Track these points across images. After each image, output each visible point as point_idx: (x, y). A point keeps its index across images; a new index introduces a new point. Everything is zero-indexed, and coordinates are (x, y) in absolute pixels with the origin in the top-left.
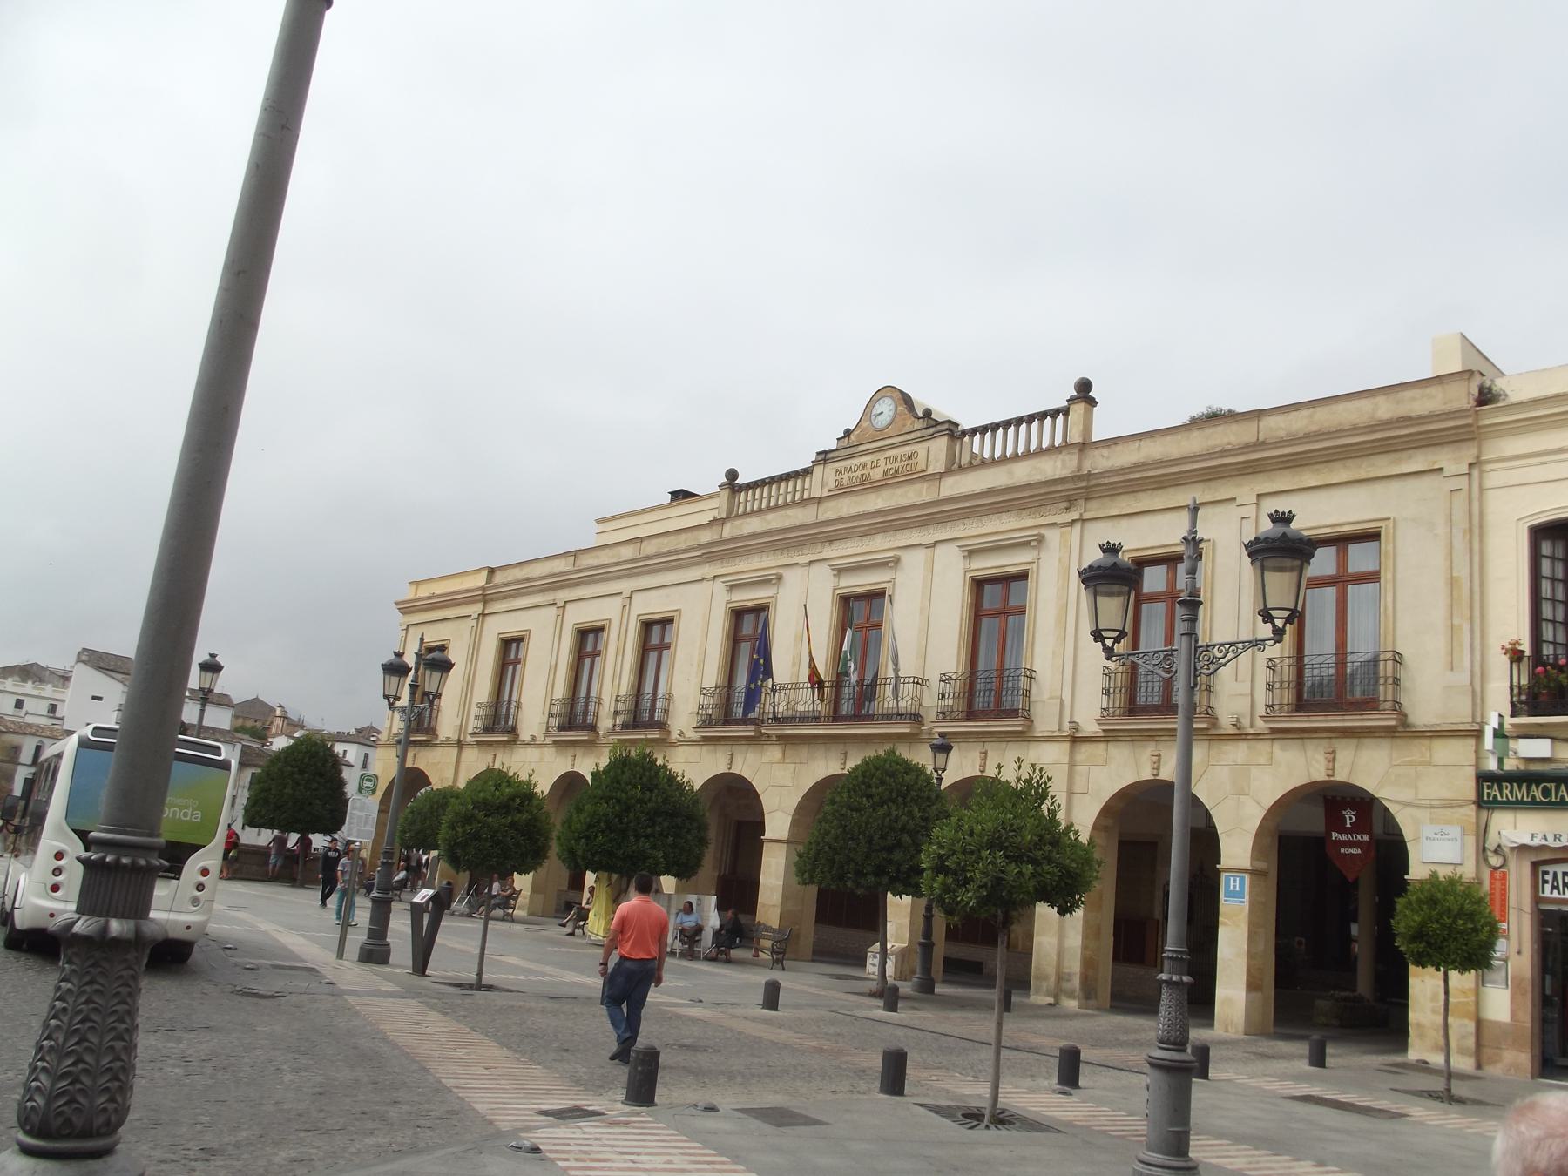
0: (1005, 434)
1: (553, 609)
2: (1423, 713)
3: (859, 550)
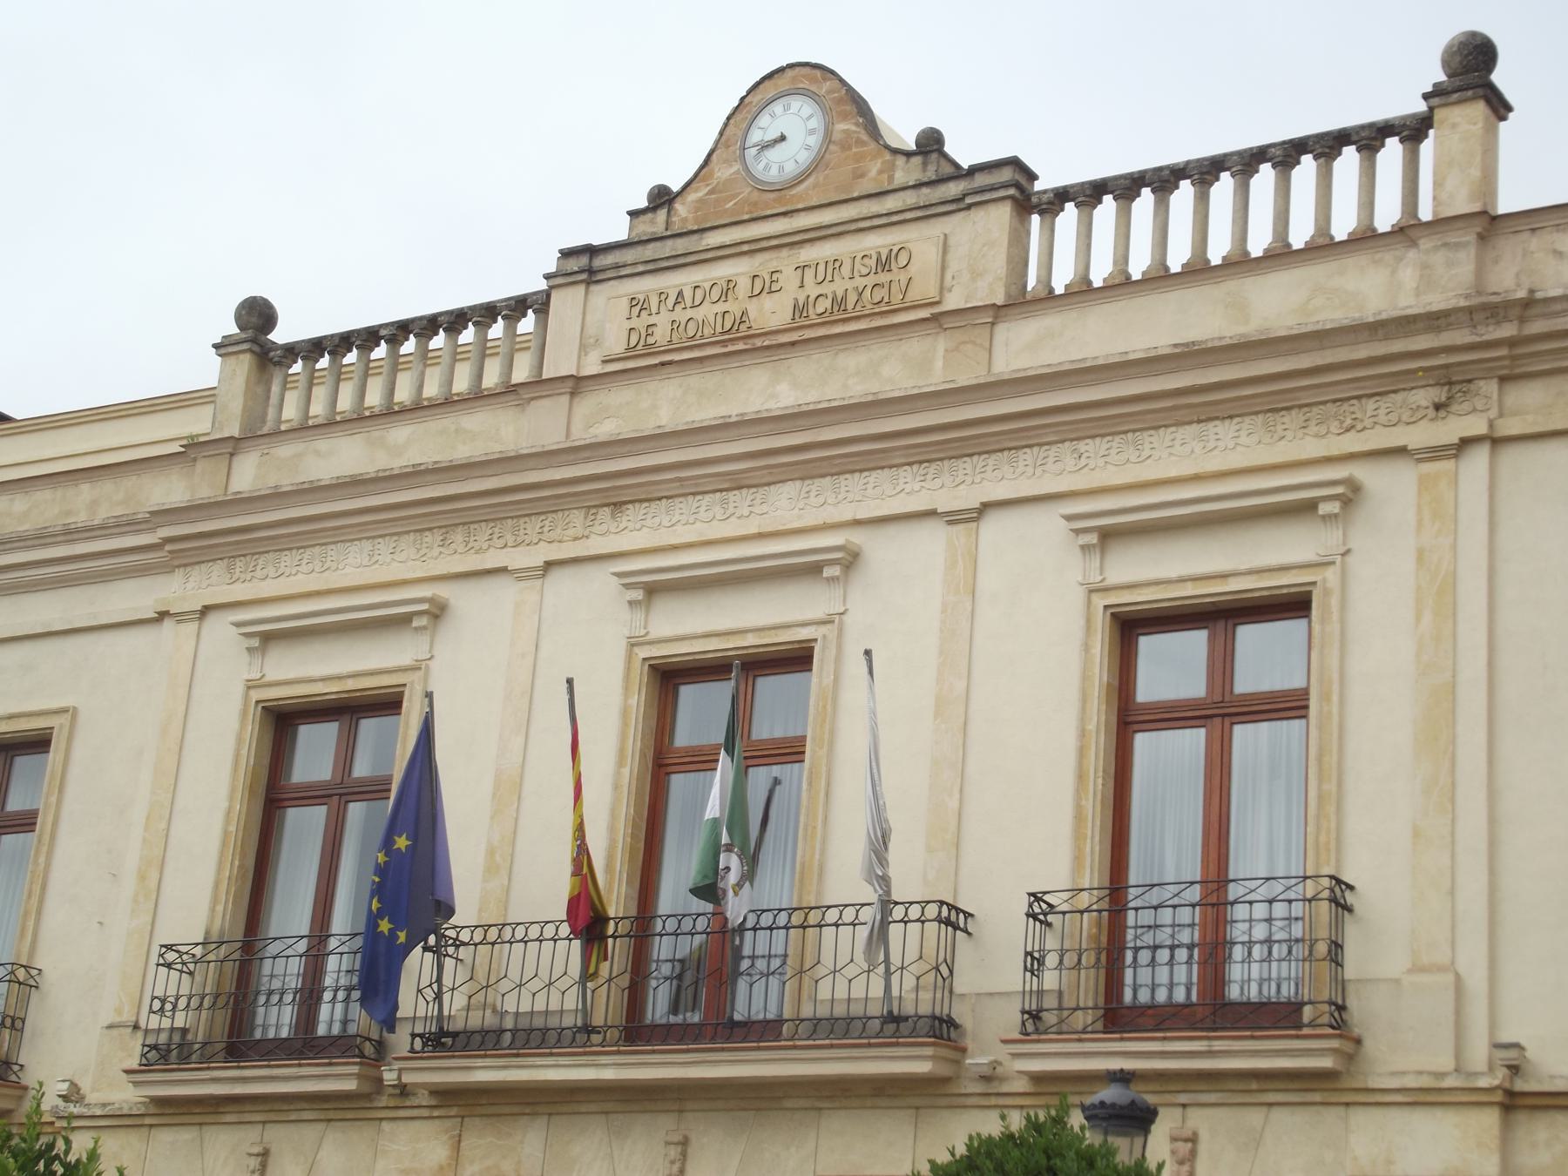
0: (1122, 257)
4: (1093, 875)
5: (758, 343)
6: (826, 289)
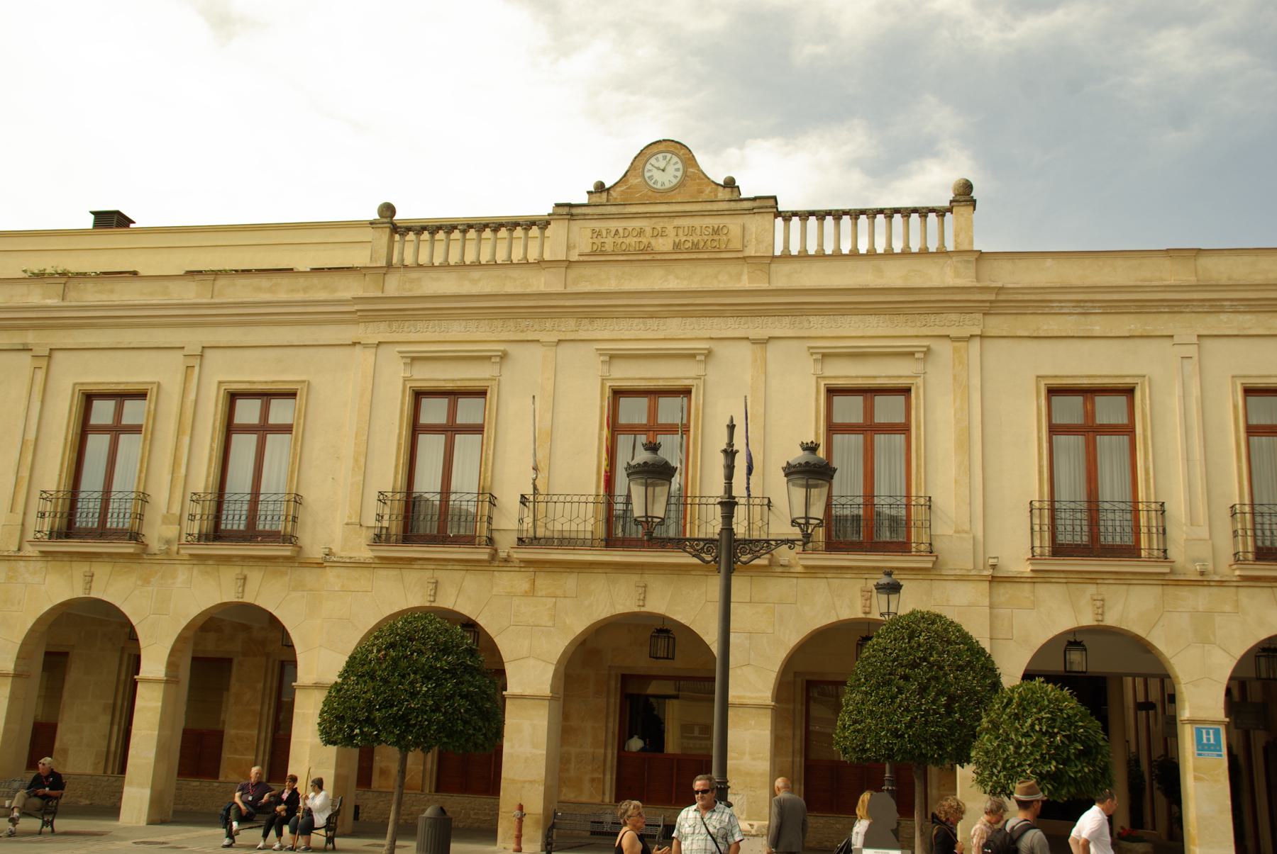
0: (821, 244)
1: (26, 358)
2: (315, 550)
3: (627, 335)
4: (65, 485)
5: (659, 257)
6: (690, 238)
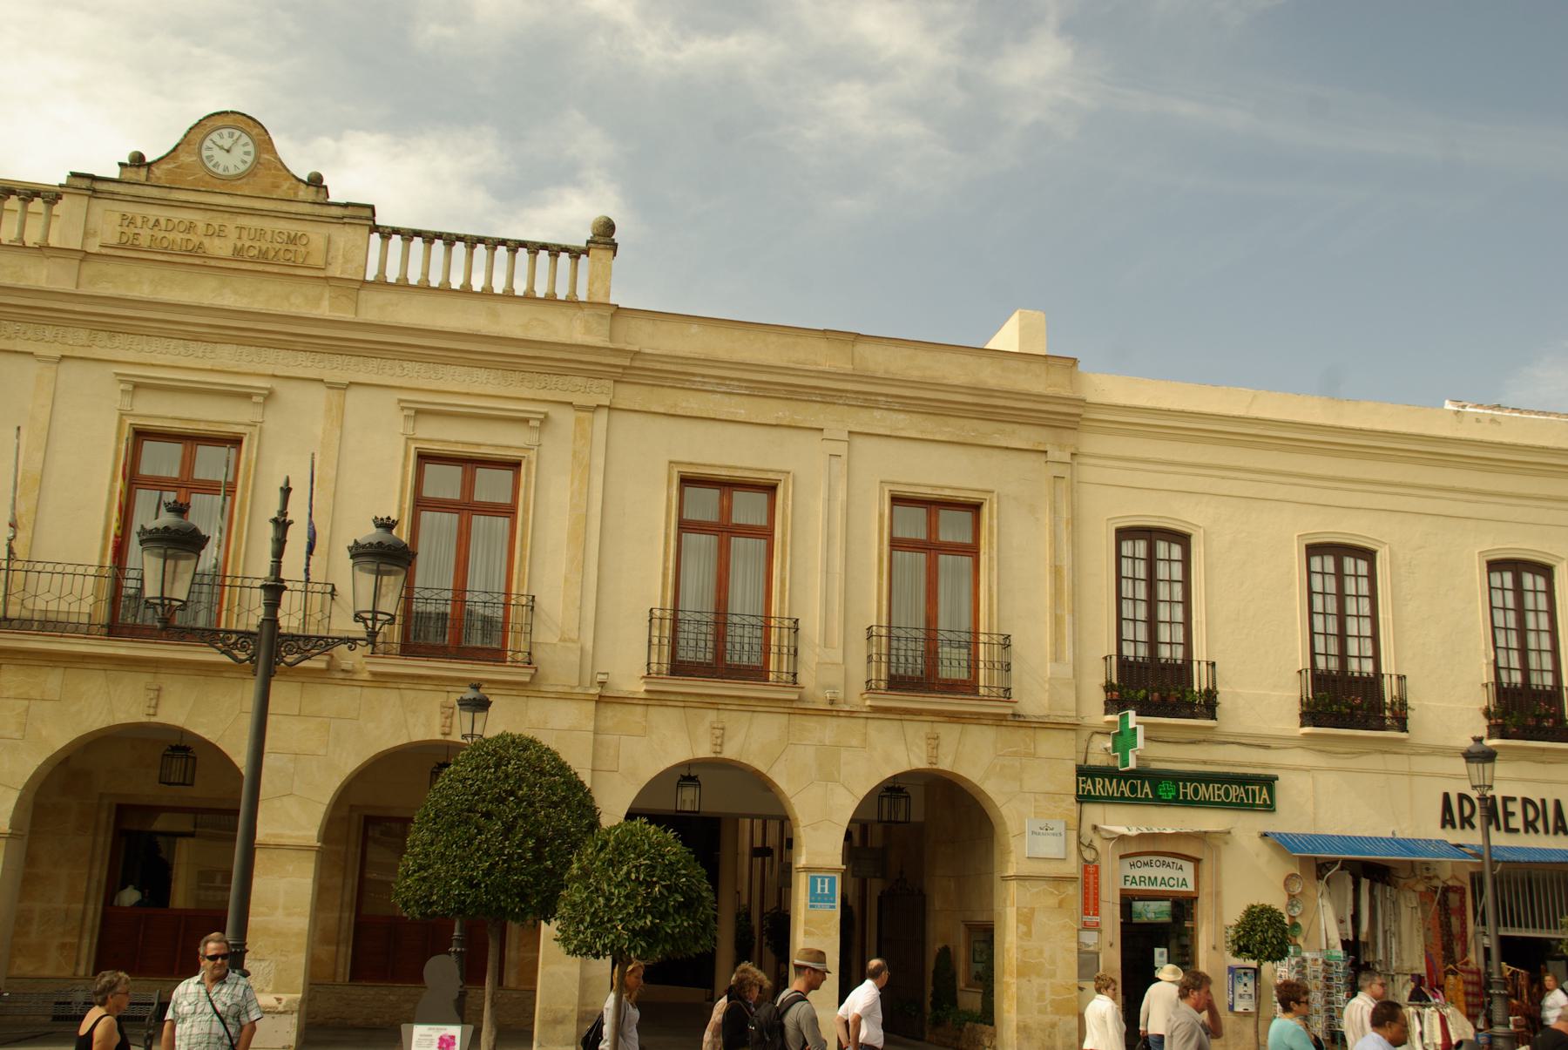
0: (426, 274)
2: (1033, 698)
5: (213, 263)
6: (257, 244)
